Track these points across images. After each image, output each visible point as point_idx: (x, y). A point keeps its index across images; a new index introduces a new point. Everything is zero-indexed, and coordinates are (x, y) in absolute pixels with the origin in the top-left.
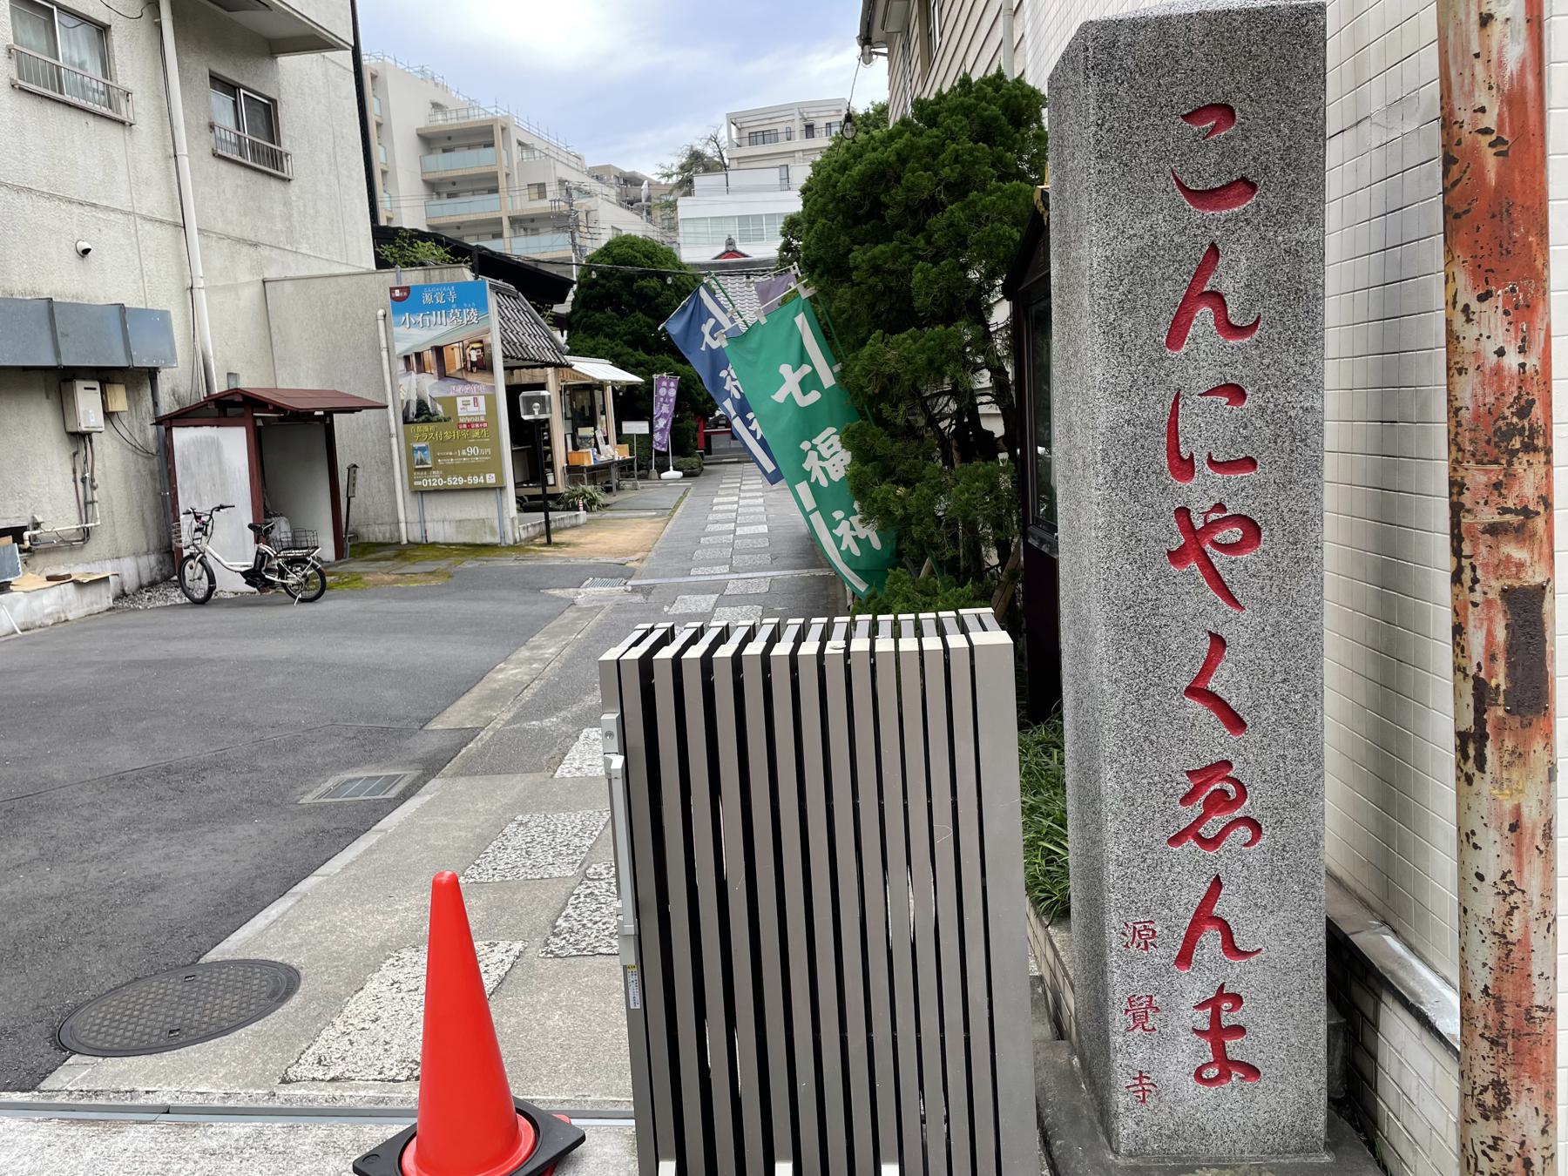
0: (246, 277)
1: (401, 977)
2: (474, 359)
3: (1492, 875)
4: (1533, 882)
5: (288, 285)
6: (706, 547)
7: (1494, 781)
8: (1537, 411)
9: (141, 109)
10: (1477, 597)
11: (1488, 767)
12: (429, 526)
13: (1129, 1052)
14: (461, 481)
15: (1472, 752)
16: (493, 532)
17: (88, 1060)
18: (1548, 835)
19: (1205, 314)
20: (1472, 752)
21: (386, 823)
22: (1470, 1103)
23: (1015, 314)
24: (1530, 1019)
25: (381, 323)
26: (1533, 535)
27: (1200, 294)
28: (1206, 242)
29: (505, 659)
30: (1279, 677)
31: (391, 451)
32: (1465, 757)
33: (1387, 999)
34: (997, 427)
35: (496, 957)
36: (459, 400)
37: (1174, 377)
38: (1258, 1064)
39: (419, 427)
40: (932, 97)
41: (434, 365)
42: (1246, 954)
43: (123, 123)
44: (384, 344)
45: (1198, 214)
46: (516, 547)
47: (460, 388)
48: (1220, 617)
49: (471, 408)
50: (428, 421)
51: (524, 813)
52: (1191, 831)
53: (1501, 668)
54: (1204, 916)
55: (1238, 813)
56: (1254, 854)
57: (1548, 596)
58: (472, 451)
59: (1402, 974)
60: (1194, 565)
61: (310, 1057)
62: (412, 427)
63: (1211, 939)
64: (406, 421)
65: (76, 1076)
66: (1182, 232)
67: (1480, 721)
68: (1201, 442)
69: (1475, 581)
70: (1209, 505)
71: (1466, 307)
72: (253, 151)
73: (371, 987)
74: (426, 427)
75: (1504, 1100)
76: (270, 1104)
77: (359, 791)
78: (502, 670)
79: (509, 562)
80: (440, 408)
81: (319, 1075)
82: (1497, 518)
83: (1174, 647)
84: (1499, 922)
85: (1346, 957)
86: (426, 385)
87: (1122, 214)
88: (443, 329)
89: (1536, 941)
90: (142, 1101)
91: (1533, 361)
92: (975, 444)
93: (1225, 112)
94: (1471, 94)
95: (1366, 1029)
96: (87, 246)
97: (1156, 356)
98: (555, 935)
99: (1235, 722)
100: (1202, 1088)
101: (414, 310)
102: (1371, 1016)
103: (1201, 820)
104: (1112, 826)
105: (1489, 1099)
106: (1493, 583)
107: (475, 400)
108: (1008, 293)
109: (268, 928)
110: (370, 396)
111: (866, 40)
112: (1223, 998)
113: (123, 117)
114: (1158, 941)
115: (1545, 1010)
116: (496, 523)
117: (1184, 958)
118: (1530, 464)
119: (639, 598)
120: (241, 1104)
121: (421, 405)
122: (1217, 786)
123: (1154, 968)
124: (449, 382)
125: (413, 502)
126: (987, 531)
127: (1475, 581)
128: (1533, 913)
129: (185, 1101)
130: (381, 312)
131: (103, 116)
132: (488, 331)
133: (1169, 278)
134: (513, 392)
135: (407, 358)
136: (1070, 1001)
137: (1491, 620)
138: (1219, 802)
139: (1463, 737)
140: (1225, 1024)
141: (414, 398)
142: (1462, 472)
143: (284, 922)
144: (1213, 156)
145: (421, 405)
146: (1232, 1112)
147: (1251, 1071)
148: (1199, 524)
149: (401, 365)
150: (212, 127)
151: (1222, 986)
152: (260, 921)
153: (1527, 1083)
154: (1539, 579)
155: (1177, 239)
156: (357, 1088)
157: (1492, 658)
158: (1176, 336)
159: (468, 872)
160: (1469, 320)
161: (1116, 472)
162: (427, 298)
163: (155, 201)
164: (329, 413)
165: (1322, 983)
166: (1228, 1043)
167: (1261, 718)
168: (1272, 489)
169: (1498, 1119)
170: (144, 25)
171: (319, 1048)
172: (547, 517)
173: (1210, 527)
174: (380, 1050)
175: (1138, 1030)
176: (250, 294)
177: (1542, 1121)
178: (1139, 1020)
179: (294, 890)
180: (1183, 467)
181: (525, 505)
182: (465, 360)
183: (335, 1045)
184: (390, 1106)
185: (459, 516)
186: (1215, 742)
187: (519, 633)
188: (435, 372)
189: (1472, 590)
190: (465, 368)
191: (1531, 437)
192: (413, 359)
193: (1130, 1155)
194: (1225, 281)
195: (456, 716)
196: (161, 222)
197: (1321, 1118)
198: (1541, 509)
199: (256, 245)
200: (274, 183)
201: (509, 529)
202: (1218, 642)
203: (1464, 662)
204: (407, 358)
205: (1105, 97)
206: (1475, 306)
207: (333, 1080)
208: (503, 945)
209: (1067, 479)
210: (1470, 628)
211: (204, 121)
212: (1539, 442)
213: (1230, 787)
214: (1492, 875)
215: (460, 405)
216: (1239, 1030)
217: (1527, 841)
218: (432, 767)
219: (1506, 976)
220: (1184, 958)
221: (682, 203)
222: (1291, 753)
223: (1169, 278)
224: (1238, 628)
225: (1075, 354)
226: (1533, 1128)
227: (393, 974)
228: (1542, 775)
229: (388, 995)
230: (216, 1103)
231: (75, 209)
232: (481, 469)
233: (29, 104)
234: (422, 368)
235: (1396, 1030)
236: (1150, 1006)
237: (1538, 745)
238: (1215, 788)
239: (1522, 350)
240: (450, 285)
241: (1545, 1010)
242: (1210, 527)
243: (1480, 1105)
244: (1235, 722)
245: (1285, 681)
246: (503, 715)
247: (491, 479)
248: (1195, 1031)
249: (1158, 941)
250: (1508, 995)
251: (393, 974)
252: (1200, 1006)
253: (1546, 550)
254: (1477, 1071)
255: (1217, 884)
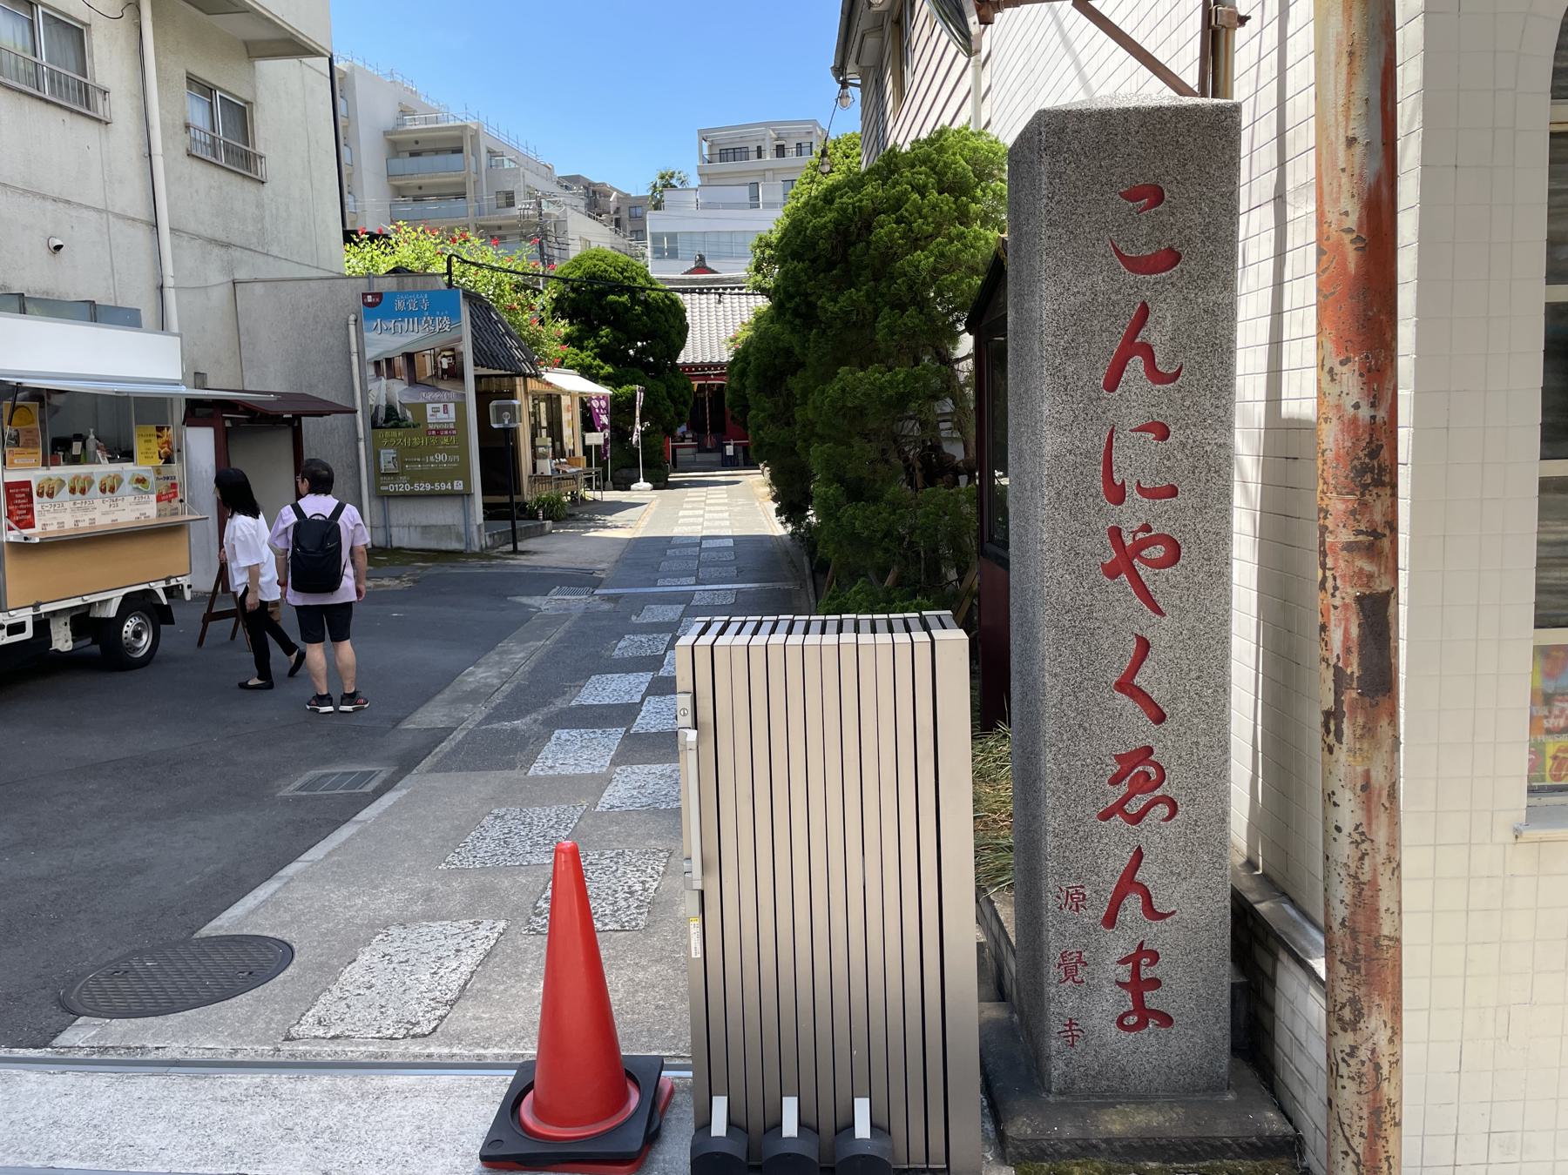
0: (216, 276)
1: (391, 951)
2: (445, 366)
3: (1348, 828)
4: (1381, 835)
5: (258, 286)
6: (672, 558)
7: (1349, 750)
8: (1385, 454)
9: (120, 107)
10: (1337, 601)
11: (1345, 739)
12: (394, 531)
13: (1061, 1001)
14: (408, 488)
15: (1332, 728)
16: (459, 539)
17: (97, 1021)
18: (1393, 794)
19: (1136, 364)
20: (1332, 728)
21: (362, 816)
22: (1333, 1018)
23: (978, 345)
24: (1377, 944)
25: (352, 328)
26: (1380, 553)
27: (1133, 346)
28: (1139, 301)
29: (474, 663)
30: (1193, 675)
31: (358, 456)
32: (1328, 731)
33: (1283, 956)
34: (957, 451)
35: (481, 933)
36: (429, 407)
37: (1110, 415)
38: (1171, 1013)
39: (387, 433)
40: (907, 147)
41: (405, 371)
42: (1163, 916)
43: (99, 121)
44: (354, 348)
45: (1131, 277)
46: (483, 554)
47: (430, 395)
48: (1144, 622)
49: (441, 415)
50: (396, 426)
51: (499, 806)
52: (1119, 807)
53: (1355, 659)
54: (1128, 883)
55: (1158, 792)
56: (1170, 829)
57: (1392, 602)
58: (441, 457)
59: (1295, 935)
60: (1124, 577)
61: (310, 1018)
62: (380, 431)
63: (1133, 903)
64: (374, 425)
65: (81, 1035)
66: (1118, 292)
67: (1338, 701)
68: (1131, 471)
69: (1336, 588)
70: (1136, 525)
71: (1331, 370)
72: (227, 151)
73: (363, 959)
74: (394, 433)
75: (1358, 1015)
76: (275, 1059)
77: (335, 786)
78: (471, 674)
79: (475, 568)
80: (409, 414)
81: (320, 1033)
82: (1353, 538)
83: (1106, 646)
84: (1353, 866)
85: (1250, 923)
86: (397, 391)
87: (1067, 274)
88: (415, 336)
89: (1384, 882)
90: (151, 1057)
91: (1382, 414)
92: (936, 469)
93: (1157, 196)
94: (1337, 200)
95: (1266, 985)
96: (59, 242)
97: (1094, 395)
98: (537, 915)
99: (1159, 718)
100: (1123, 1034)
101: (386, 317)
102: (1269, 973)
103: (1126, 799)
104: (1050, 802)
105: (1347, 1014)
106: (1349, 590)
107: (445, 407)
108: (969, 329)
109: (257, 908)
110: (338, 399)
111: (839, 70)
112: (1142, 955)
113: (100, 115)
114: (1087, 904)
115: (1391, 939)
116: (462, 530)
117: (1110, 920)
118: (1378, 496)
119: (606, 606)
120: (247, 1059)
121: (390, 409)
122: (1140, 768)
123: (1084, 927)
124: (419, 388)
125: (377, 504)
126: (945, 551)
127: (1336, 588)
128: (1380, 859)
129: (194, 1055)
130: (352, 317)
131: (79, 113)
132: (460, 339)
133: (1107, 330)
134: (483, 398)
135: (377, 364)
136: (1012, 965)
137: (1347, 620)
138: (1145, 784)
139: (1328, 715)
140: (1144, 977)
141: (383, 403)
142: (1326, 501)
143: (272, 902)
144: (1145, 229)
145: (390, 409)
146: (1146, 1051)
147: (1166, 1020)
148: (1128, 542)
149: (371, 371)
150: (187, 127)
151: (1142, 944)
152: (250, 901)
153: (1377, 1000)
154: (1385, 588)
155: (1113, 297)
156: (357, 1045)
157: (1348, 650)
158: (1112, 383)
159: (449, 859)
160: (1333, 380)
161: (1059, 494)
162: (400, 305)
163: (131, 199)
164: (297, 417)
165: (1228, 940)
166: (1146, 994)
167: (1178, 710)
168: (1191, 512)
169: (1354, 1030)
170: (123, 27)
171: (318, 1010)
172: (513, 525)
173: (1140, 546)
174: (376, 1013)
175: (1069, 982)
176: (220, 295)
177: (1389, 1033)
178: (1070, 973)
179: (281, 873)
180: (1117, 494)
181: (491, 512)
182: (436, 367)
183: (333, 1008)
184: (389, 1060)
185: (425, 523)
186: (1137, 729)
187: (485, 641)
188: (405, 378)
189: (1333, 595)
190: (435, 375)
191: (1380, 474)
192: (384, 365)
193: (1061, 1093)
194: (1152, 335)
195: (431, 716)
196: (134, 219)
197: (1225, 1060)
198: (1387, 532)
199: (227, 245)
200: (248, 185)
201: (475, 535)
202: (1144, 646)
203: (1327, 654)
204: (377, 364)
205: (1055, 175)
206: (1338, 369)
207: (333, 1038)
208: (487, 924)
209: (1018, 499)
210: (1332, 627)
211: (180, 123)
212: (1386, 479)
213: (1151, 770)
214: (1348, 828)
215: (429, 412)
216: (1155, 983)
217: (1375, 798)
218: (406, 764)
219: (1360, 910)
220: (1110, 920)
221: (651, 215)
222: (1203, 740)
223: (1107, 330)
224: (1159, 632)
225: (1026, 392)
226: (1382, 1037)
227: (383, 948)
228: (1386, 747)
229: (380, 966)
230: (224, 1058)
231: (49, 205)
232: (448, 476)
233: (198, 167)
234: (392, 374)
235: (1290, 981)
236: (1079, 961)
237: (1384, 722)
238: (1138, 769)
239: (1373, 405)
240: (424, 293)
241: (1391, 939)
242: (1140, 546)
243: (1340, 1019)
244: (1159, 718)
245: (1198, 678)
246: (474, 715)
247: (459, 486)
248: (1117, 982)
249: (1087, 904)
250: (1361, 926)
251: (383, 948)
252: (1123, 962)
253: (1390, 565)
254: (1338, 991)
255: (1139, 855)
